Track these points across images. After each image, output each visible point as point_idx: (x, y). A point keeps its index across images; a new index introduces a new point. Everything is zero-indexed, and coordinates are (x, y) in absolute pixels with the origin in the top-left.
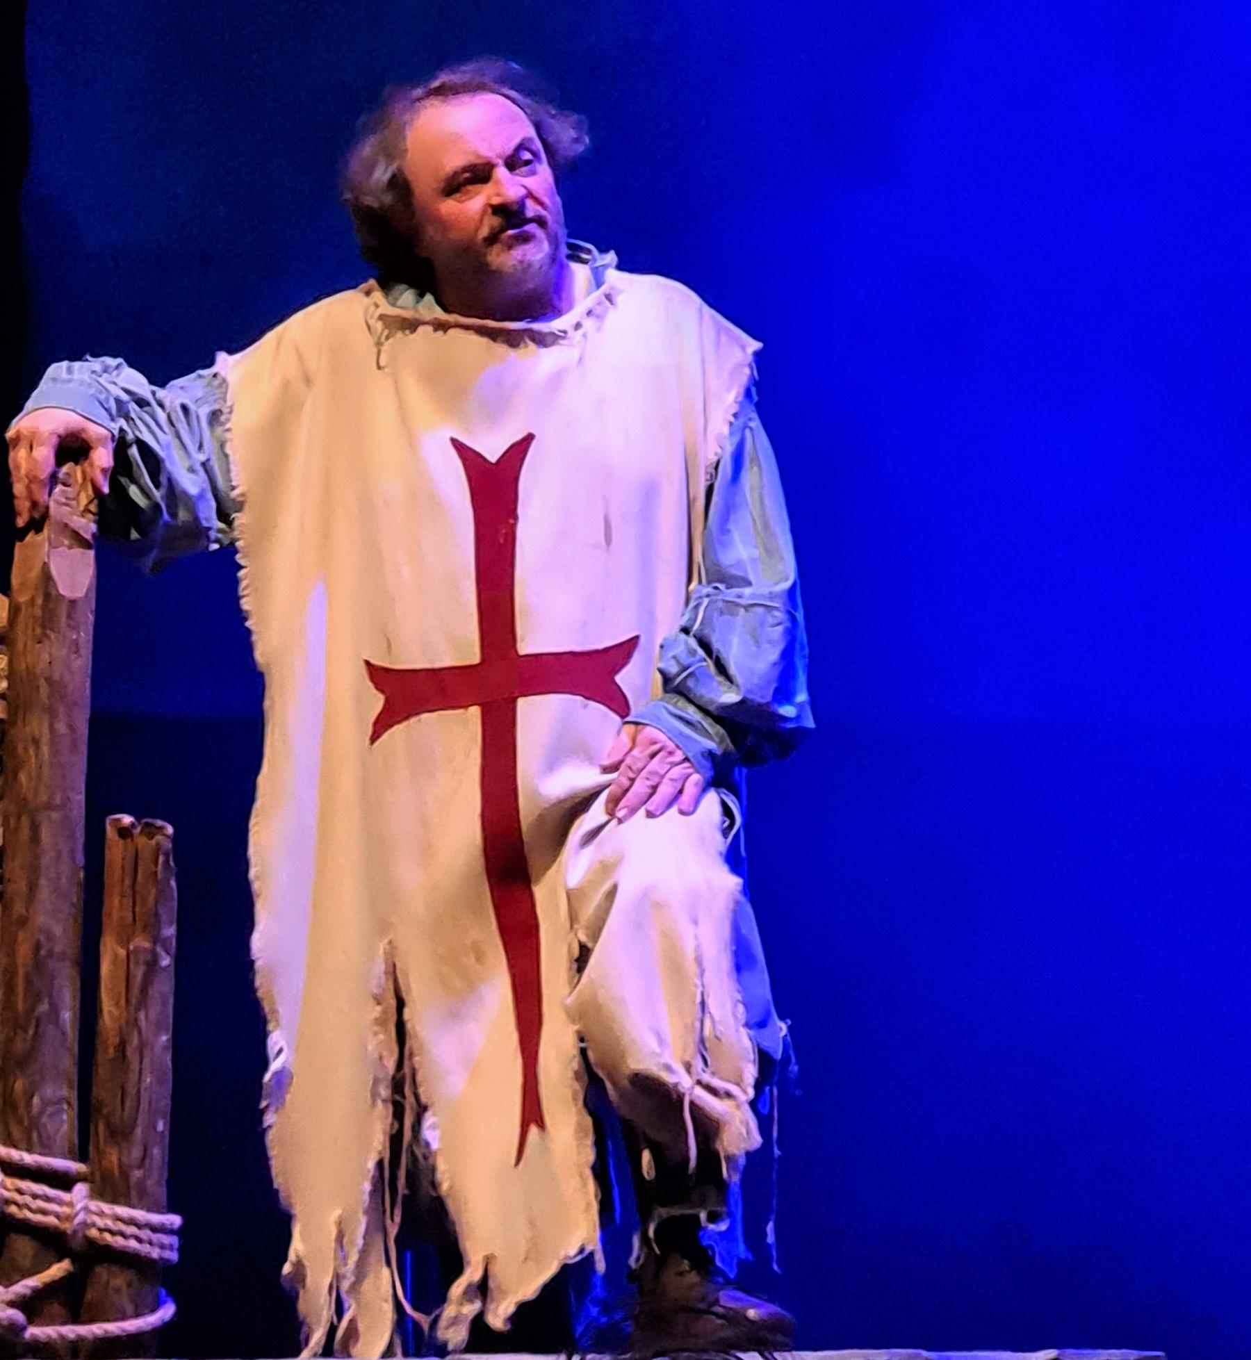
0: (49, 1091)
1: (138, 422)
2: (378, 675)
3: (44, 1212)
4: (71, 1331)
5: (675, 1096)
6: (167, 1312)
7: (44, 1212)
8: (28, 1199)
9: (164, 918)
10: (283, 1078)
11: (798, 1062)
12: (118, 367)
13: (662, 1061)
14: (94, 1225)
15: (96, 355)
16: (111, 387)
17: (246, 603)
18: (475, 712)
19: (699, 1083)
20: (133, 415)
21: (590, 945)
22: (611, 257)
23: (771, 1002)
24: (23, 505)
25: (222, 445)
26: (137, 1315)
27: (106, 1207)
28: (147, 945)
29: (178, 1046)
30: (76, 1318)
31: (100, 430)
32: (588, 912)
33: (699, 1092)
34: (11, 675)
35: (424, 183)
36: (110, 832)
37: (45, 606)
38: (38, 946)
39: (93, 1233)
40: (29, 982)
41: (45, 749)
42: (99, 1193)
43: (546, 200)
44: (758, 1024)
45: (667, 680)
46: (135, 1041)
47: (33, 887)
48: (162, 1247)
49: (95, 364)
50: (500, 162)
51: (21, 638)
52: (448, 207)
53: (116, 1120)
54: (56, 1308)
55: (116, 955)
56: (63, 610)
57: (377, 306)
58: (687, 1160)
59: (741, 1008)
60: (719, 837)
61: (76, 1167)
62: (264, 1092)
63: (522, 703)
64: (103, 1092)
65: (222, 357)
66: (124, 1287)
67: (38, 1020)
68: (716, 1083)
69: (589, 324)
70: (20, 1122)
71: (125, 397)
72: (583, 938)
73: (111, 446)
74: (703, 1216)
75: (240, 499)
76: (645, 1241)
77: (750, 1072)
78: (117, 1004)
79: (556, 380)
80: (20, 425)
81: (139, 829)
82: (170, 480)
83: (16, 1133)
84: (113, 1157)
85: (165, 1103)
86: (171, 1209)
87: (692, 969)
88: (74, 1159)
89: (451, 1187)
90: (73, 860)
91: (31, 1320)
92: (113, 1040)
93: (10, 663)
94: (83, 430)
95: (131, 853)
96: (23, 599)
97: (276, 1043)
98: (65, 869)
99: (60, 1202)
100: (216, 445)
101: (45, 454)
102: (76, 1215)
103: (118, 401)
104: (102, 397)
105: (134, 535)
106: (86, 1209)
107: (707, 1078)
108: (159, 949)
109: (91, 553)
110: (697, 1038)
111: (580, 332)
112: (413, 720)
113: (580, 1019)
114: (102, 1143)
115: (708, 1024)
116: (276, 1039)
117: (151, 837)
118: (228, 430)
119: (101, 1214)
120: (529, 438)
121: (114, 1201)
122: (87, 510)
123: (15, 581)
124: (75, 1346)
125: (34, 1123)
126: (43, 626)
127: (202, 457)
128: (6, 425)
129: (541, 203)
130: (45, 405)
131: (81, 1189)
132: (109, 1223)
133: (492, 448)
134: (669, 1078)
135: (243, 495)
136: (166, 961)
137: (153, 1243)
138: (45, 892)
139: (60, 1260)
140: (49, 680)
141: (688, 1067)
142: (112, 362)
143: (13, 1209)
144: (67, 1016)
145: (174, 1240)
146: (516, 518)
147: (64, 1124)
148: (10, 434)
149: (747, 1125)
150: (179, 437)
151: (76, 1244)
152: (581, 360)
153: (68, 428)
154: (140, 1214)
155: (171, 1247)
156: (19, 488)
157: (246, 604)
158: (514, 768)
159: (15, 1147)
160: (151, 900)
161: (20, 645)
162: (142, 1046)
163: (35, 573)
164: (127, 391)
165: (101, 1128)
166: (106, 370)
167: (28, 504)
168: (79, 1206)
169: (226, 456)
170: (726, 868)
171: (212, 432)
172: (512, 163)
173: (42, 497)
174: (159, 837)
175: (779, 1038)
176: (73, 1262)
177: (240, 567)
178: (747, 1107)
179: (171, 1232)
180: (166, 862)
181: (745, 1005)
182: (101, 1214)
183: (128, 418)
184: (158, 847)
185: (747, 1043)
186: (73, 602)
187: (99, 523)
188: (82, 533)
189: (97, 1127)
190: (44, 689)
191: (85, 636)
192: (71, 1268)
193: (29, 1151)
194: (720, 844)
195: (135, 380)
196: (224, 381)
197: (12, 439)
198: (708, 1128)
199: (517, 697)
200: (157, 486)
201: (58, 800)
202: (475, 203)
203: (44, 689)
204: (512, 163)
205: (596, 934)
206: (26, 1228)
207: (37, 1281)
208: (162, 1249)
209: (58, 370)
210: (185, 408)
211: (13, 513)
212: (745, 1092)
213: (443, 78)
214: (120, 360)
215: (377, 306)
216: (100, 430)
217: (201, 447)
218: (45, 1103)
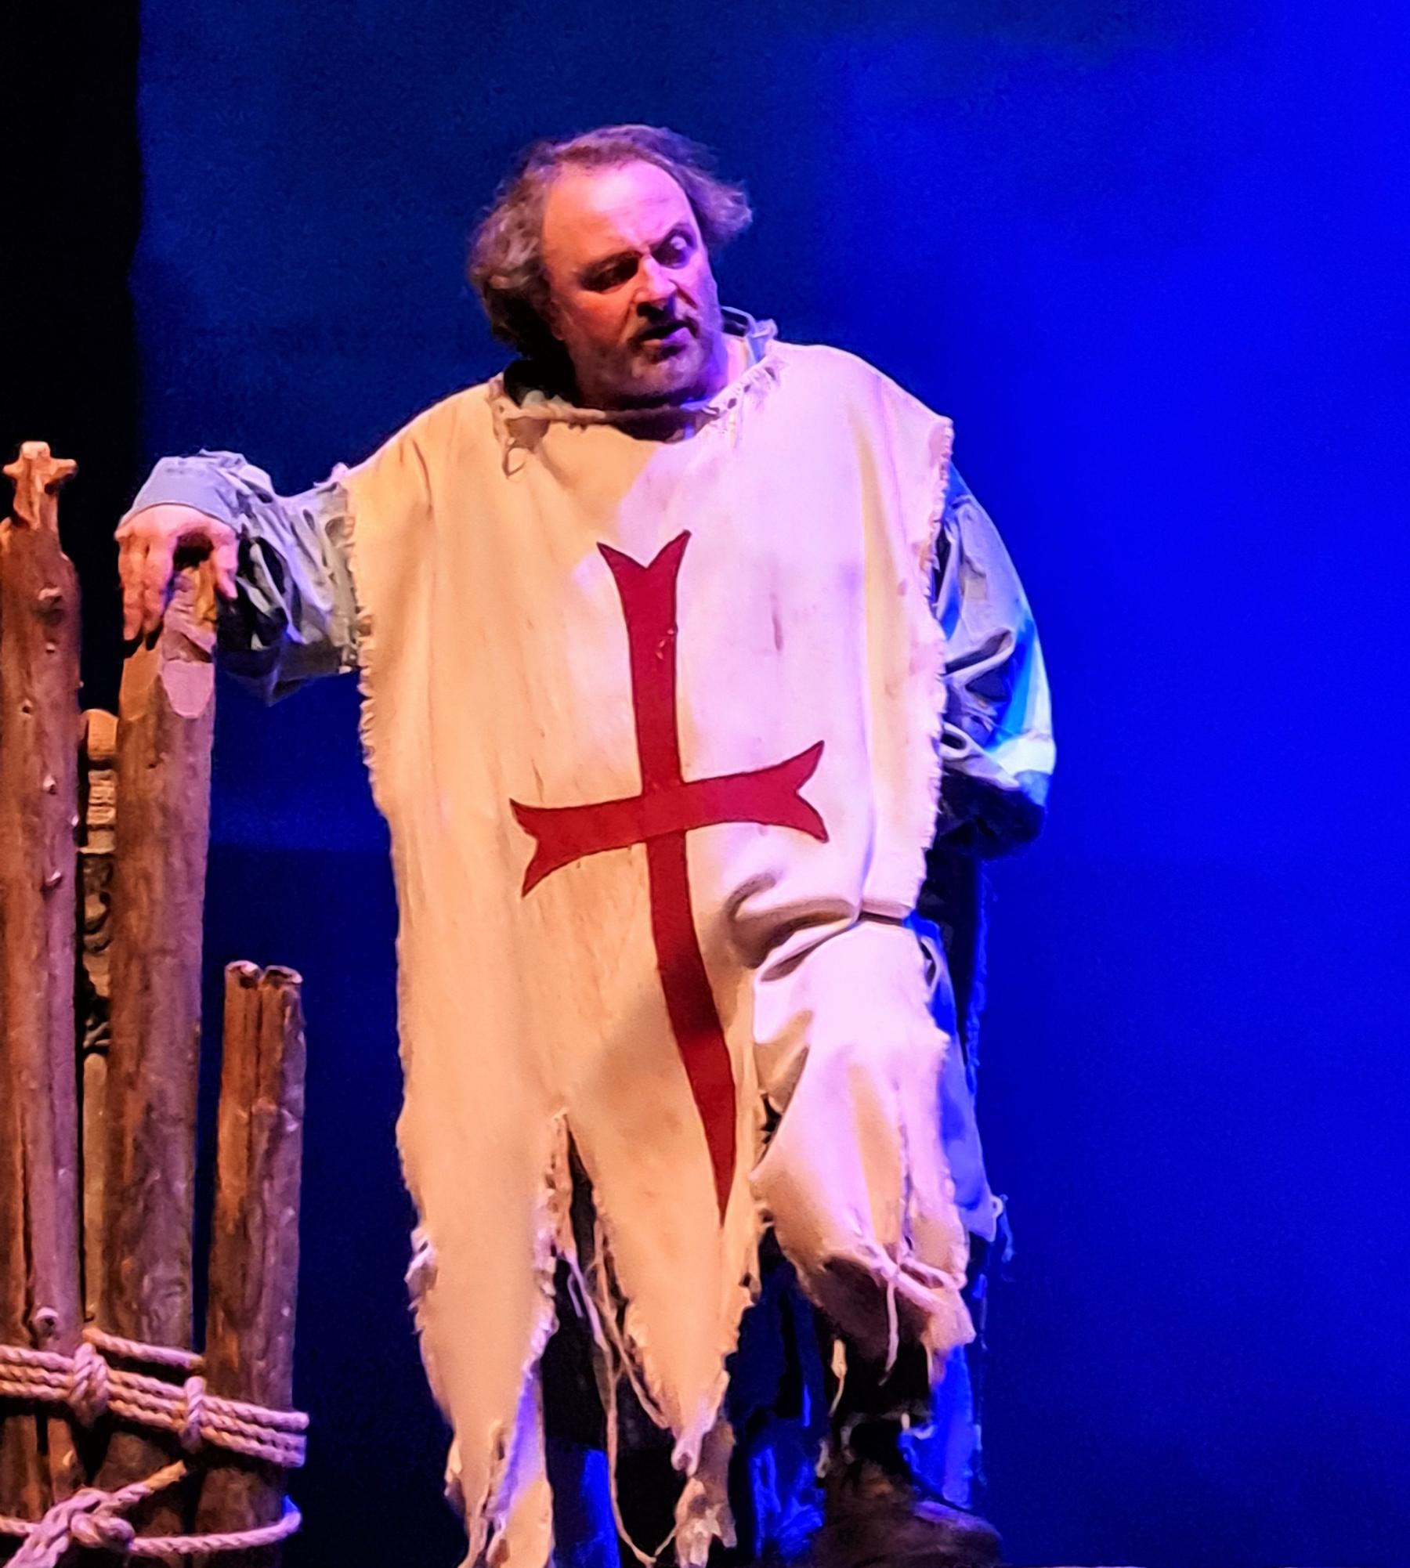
0: (160, 1271)
1: (261, 519)
6: (291, 1521)
7: (155, 1409)
8: (136, 1393)
9: (290, 1075)
11: (1015, 1246)
12: (238, 462)
13: (862, 1242)
14: (210, 1423)
17: (365, 739)
18: (639, 850)
19: (904, 1268)
20: (254, 510)
24: (132, 614)
25: (345, 562)
26: (260, 1523)
27: (225, 1405)
28: (273, 1107)
33: (906, 1281)
35: (564, 270)
36: (230, 978)
37: (159, 725)
38: (149, 1109)
39: (210, 1432)
40: (138, 1147)
41: (159, 887)
42: (217, 1387)
43: (697, 299)
44: (970, 1204)
48: (287, 1447)
50: (646, 250)
52: (588, 298)
53: (236, 1305)
55: (237, 1118)
58: (886, 1353)
59: (950, 1185)
60: (923, 984)
61: (190, 1358)
64: (220, 1271)
66: (245, 1494)
67: (151, 1191)
68: (922, 1268)
70: (128, 1306)
71: (246, 490)
73: (236, 544)
74: (905, 1420)
75: (367, 622)
76: (836, 1451)
77: (961, 1257)
78: (237, 1173)
81: (262, 978)
82: (295, 587)
83: (124, 1319)
84: (232, 1347)
85: (290, 1286)
86: (298, 1406)
87: (897, 1139)
88: (186, 1349)
89: (663, 1389)
90: (189, 1013)
91: (139, 1532)
92: (234, 1213)
94: (205, 528)
95: (255, 1003)
98: (179, 1020)
99: (172, 1398)
101: (162, 560)
104: (223, 490)
105: (256, 643)
106: (202, 1405)
107: (912, 1263)
108: (285, 1112)
109: (210, 668)
110: (901, 1218)
113: (768, 1198)
114: (220, 1329)
117: (277, 985)
118: (352, 545)
119: (218, 1411)
121: (234, 1397)
122: (206, 619)
123: (123, 697)
125: (144, 1309)
126: (158, 751)
128: (115, 525)
129: (690, 301)
130: (163, 502)
131: (195, 1384)
132: (229, 1422)
134: (870, 1263)
135: (369, 617)
136: (293, 1126)
137: (204, 1424)
138: (157, 1050)
139: (171, 1463)
143: (119, 1405)
144: (182, 1186)
145: (300, 1441)
147: (177, 1308)
148: (120, 533)
149: (957, 1313)
150: (300, 544)
151: (189, 1444)
154: (262, 1412)
155: (297, 1449)
156: (130, 596)
157: (367, 740)
158: (689, 911)
159: (123, 1336)
160: (278, 1056)
161: (130, 772)
165: (221, 1315)
168: (193, 1402)
169: (350, 574)
170: (931, 1021)
171: (333, 543)
172: (666, 253)
173: (156, 606)
175: (992, 1219)
176: (186, 1465)
177: (364, 698)
179: (298, 1432)
180: (293, 1015)
181: (955, 1180)
182: (218, 1411)
183: (250, 516)
184: (285, 995)
186: (192, 721)
187: (220, 635)
188: (199, 643)
190: (158, 820)
191: (203, 759)
192: (184, 1471)
193: (140, 1340)
194: (924, 994)
197: (122, 538)
198: (914, 1318)
199: (686, 831)
200: (282, 590)
202: (617, 299)
203: (158, 820)
204: (666, 253)
205: (786, 1098)
207: (147, 1487)
208: (288, 1451)
210: (308, 516)
211: (120, 621)
212: (955, 1279)
216: (223, 526)
218: (156, 1284)
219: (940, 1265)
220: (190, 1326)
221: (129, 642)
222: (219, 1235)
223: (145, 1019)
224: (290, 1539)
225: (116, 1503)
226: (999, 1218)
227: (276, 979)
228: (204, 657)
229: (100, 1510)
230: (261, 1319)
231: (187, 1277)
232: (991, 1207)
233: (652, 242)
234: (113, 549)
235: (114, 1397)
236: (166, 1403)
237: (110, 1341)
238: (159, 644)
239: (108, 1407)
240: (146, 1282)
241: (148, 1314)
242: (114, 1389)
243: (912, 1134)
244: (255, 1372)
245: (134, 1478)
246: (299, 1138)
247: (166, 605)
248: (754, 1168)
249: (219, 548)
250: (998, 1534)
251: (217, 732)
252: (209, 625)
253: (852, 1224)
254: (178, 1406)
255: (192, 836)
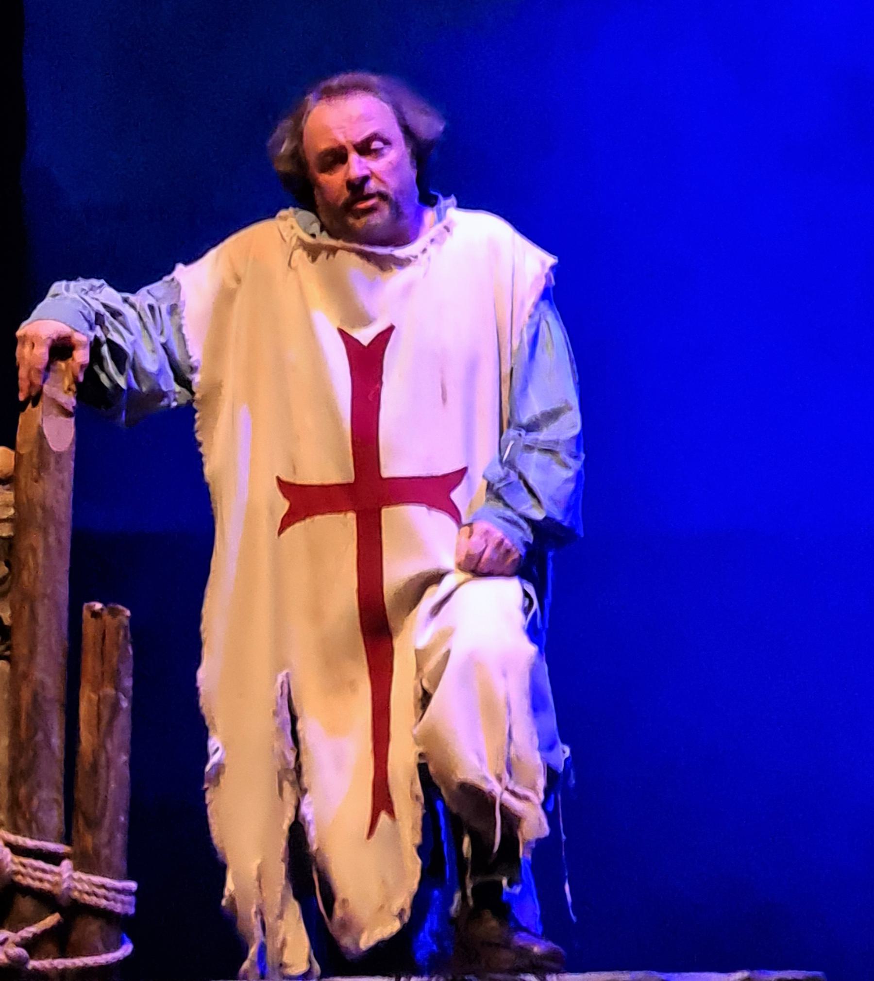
2: (285, 487)
3: (41, 880)
4: (61, 963)
5: (489, 799)
6: (126, 950)
8: (30, 871)
10: (219, 768)
12: (100, 287)
13: (481, 774)
14: (76, 887)
15: (87, 277)
16: (94, 303)
18: (351, 516)
19: (507, 789)
20: (107, 324)
21: (430, 691)
22: (453, 200)
23: (557, 733)
24: (23, 384)
25: (180, 328)
26: (108, 951)
27: (85, 877)
28: (113, 692)
29: (133, 763)
30: (63, 954)
31: (82, 337)
32: (431, 665)
33: (507, 796)
34: (17, 505)
36: (86, 614)
39: (76, 894)
41: (40, 554)
42: (79, 866)
44: (547, 747)
45: (490, 487)
46: (103, 759)
47: (32, 652)
49: (83, 284)
51: (23, 479)
54: (50, 947)
56: (52, 461)
57: (292, 228)
61: (63, 848)
62: (206, 777)
63: (385, 511)
64: (81, 794)
65: (180, 267)
68: (518, 789)
69: (432, 249)
71: (102, 310)
72: (426, 685)
74: (505, 882)
78: (91, 733)
79: (408, 289)
80: (25, 329)
83: (21, 823)
84: (89, 841)
85: (124, 803)
86: (129, 877)
88: (61, 842)
91: (32, 956)
93: (16, 497)
96: (23, 451)
97: (214, 745)
100: (174, 329)
101: (42, 353)
102: (64, 882)
103: (98, 314)
104: (86, 312)
109: (72, 420)
111: (426, 256)
112: (308, 520)
113: (424, 744)
115: (512, 748)
116: (214, 742)
119: (80, 880)
120: (391, 329)
122: (69, 389)
123: (19, 439)
124: (63, 973)
127: (163, 340)
128: (17, 327)
131: (66, 864)
132: (87, 888)
133: (365, 336)
134: (485, 787)
136: (125, 704)
138: (40, 659)
140: (44, 508)
141: (500, 779)
142: (96, 282)
143: (19, 878)
144: (57, 741)
145: (131, 899)
146: (381, 383)
147: (54, 818)
148: (19, 333)
151: (64, 902)
152: (425, 274)
153: (60, 335)
154: (107, 881)
156: (22, 373)
160: (115, 660)
161: (22, 484)
162: (108, 760)
163: (34, 431)
164: (105, 306)
165: (81, 822)
166: (92, 288)
167: (28, 383)
168: (65, 876)
169: (183, 335)
173: (38, 381)
174: (120, 617)
178: (540, 807)
180: (126, 636)
183: (102, 326)
185: (539, 761)
188: (66, 406)
189: (77, 821)
190: (39, 512)
191: (67, 476)
195: (110, 296)
196: (178, 284)
197: (21, 337)
198: (512, 821)
201: (49, 591)
203: (39, 512)
206: (28, 891)
208: (123, 906)
209: (58, 287)
211: (17, 390)
213: (335, 82)
214: (102, 281)
215: (292, 228)
216: (82, 337)
217: (162, 333)
219: (530, 787)
220: (63, 826)
221: (22, 402)
222: (79, 768)
223: (33, 635)
224: (126, 960)
225: (18, 939)
226: (566, 760)
227: (114, 613)
228: (67, 414)
229: (9, 944)
230: (107, 822)
231: (60, 798)
232: (561, 752)
233: (354, 143)
234: (13, 342)
235: (18, 873)
236: (48, 877)
237: (12, 838)
238: (40, 403)
239: (12, 881)
240: (35, 802)
241: (36, 822)
242: (14, 868)
243: (514, 707)
244: (103, 858)
245: (30, 923)
246: (129, 712)
247: (44, 381)
248: (416, 725)
249: (79, 349)
250: (562, 950)
251: (76, 461)
252: (71, 393)
253: (473, 760)
254: (57, 878)
255: (61, 524)
